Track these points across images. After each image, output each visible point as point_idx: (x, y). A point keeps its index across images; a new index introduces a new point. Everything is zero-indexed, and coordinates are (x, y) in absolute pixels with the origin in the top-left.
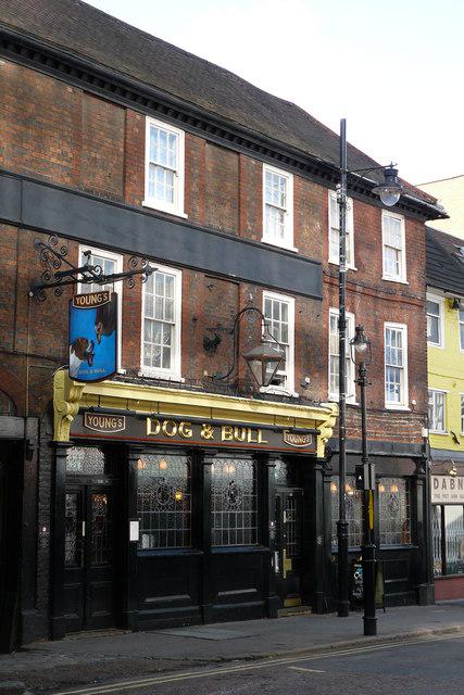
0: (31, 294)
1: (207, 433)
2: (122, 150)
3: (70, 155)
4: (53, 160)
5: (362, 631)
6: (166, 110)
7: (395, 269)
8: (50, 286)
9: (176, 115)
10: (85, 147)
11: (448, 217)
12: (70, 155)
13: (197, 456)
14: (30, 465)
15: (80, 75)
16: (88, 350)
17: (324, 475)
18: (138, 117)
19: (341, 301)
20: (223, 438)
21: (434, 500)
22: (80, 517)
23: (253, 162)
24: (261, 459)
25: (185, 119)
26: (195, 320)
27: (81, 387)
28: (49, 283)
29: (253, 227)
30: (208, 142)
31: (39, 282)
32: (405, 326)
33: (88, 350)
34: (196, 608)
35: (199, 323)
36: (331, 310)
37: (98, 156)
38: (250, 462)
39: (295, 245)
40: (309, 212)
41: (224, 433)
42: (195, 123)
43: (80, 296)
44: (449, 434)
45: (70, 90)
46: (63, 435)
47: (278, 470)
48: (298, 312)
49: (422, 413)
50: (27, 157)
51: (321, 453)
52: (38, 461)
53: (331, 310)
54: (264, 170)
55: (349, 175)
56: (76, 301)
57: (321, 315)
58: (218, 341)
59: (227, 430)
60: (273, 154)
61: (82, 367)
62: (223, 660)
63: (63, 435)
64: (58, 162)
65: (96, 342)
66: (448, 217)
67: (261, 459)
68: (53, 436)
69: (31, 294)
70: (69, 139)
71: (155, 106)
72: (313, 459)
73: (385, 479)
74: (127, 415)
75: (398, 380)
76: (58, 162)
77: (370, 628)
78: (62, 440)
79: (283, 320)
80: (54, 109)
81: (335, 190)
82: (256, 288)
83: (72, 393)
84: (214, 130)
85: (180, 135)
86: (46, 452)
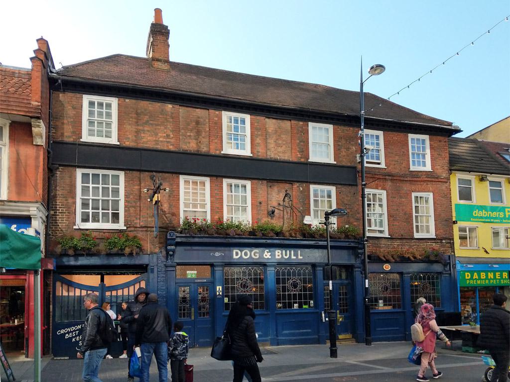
3: (172, 136)
35: (263, 204)
80: (160, 116)
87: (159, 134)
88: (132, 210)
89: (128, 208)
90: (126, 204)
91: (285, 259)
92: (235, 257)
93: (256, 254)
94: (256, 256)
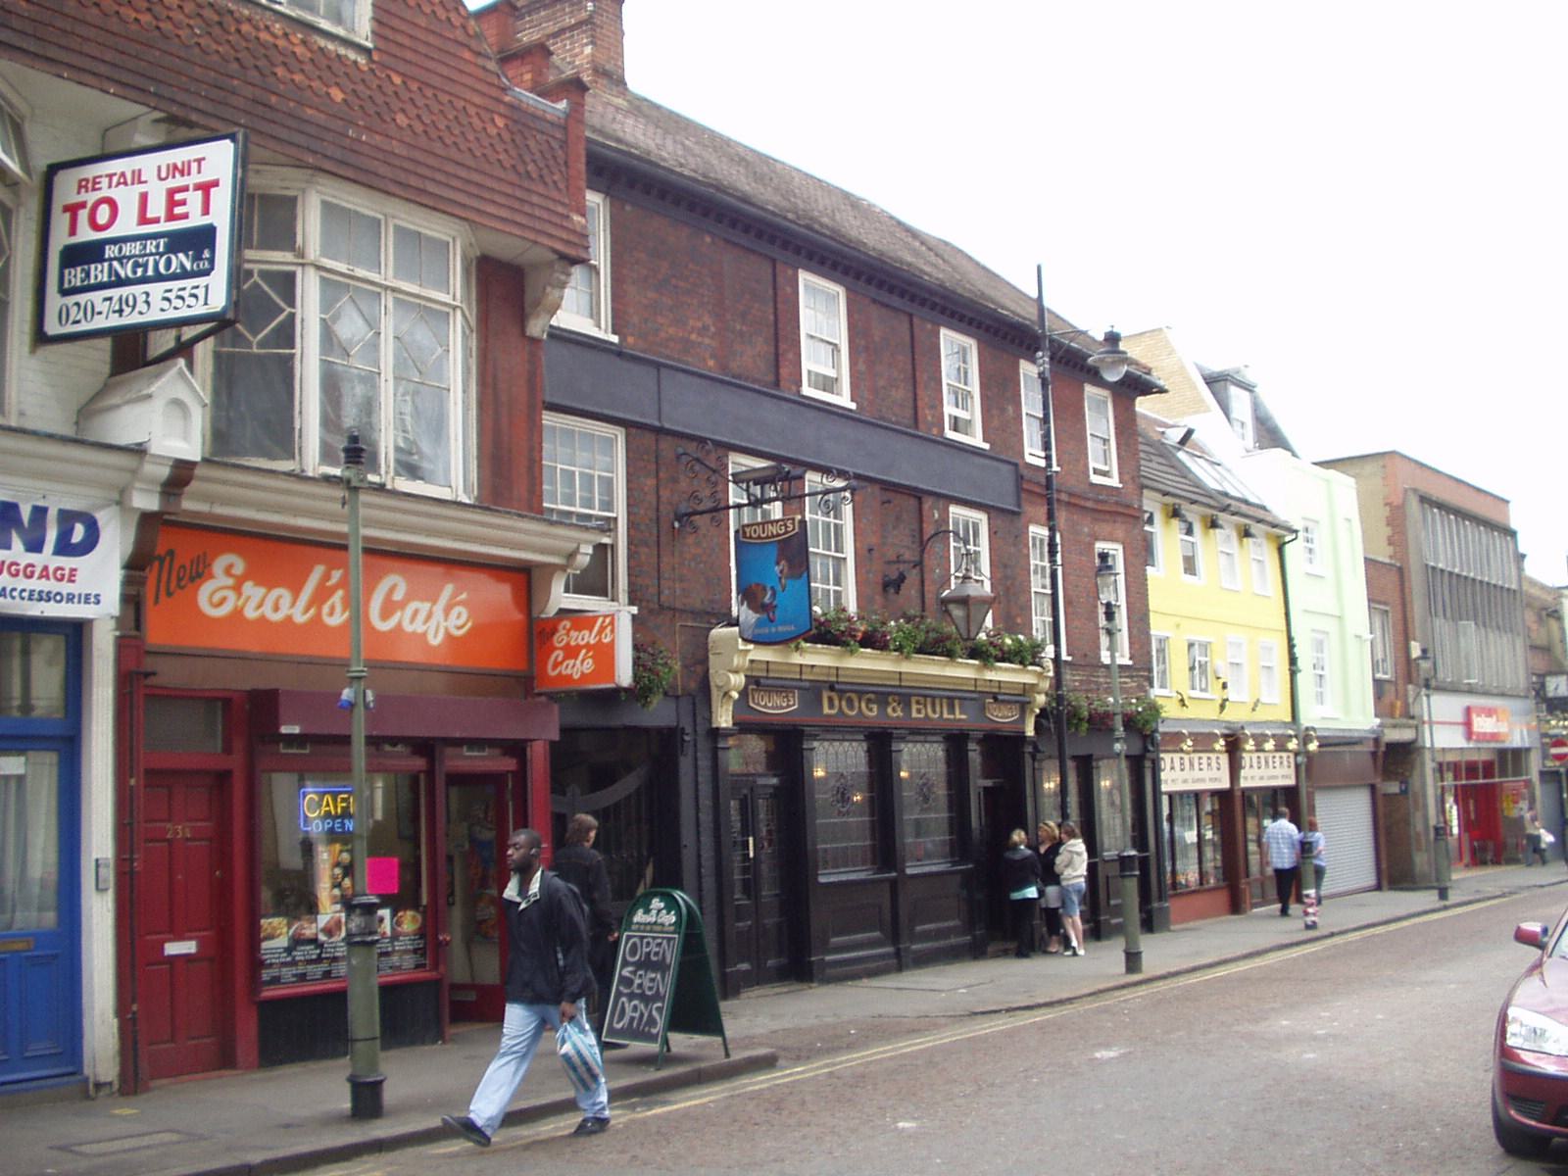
0: (677, 525)
1: (895, 712)
2: (772, 317)
4: (693, 337)
5: (1124, 970)
6: (822, 262)
7: (1103, 465)
8: (702, 513)
9: (834, 266)
10: (728, 317)
11: (1162, 391)
12: (713, 329)
13: (881, 744)
14: (685, 764)
15: (677, 202)
16: (767, 599)
17: (1034, 759)
18: (790, 272)
19: (1050, 516)
20: (914, 715)
21: (1164, 788)
22: (745, 832)
23: (929, 326)
24: (955, 742)
25: (846, 272)
26: (870, 550)
27: (748, 651)
28: (701, 508)
29: (933, 416)
30: (874, 301)
31: (684, 508)
32: (1120, 547)
33: (767, 599)
34: (890, 949)
35: (875, 554)
36: (1033, 529)
37: (744, 328)
38: (865, 745)
39: (1121, 482)
40: (999, 393)
41: (914, 707)
42: (858, 277)
43: (748, 526)
44: (1175, 694)
45: (708, 239)
46: (724, 719)
47: (975, 755)
48: (993, 533)
49: (1142, 669)
50: (663, 335)
51: (1030, 732)
52: (696, 759)
53: (1033, 529)
54: (800, 280)
55: (1052, 341)
56: (744, 533)
57: (1020, 538)
58: (902, 578)
59: (918, 703)
60: (952, 315)
61: (758, 624)
62: (913, 1031)
63: (724, 719)
64: (700, 339)
65: (779, 588)
66: (1166, 391)
67: (955, 742)
68: (710, 721)
69: (677, 525)
70: (710, 307)
71: (810, 256)
72: (1021, 738)
73: (1105, 761)
74: (799, 688)
75: (837, 582)
76: (700, 339)
77: (1133, 961)
78: (724, 725)
79: (975, 545)
80: (691, 266)
81: (1033, 361)
82: (941, 503)
83: (737, 661)
84: (881, 285)
85: (839, 291)
86: (703, 745)
87: (691, 322)
88: (644, 550)
89: (636, 546)
90: (632, 532)
91: (892, 718)
92: (826, 710)
93: (871, 706)
94: (871, 710)
